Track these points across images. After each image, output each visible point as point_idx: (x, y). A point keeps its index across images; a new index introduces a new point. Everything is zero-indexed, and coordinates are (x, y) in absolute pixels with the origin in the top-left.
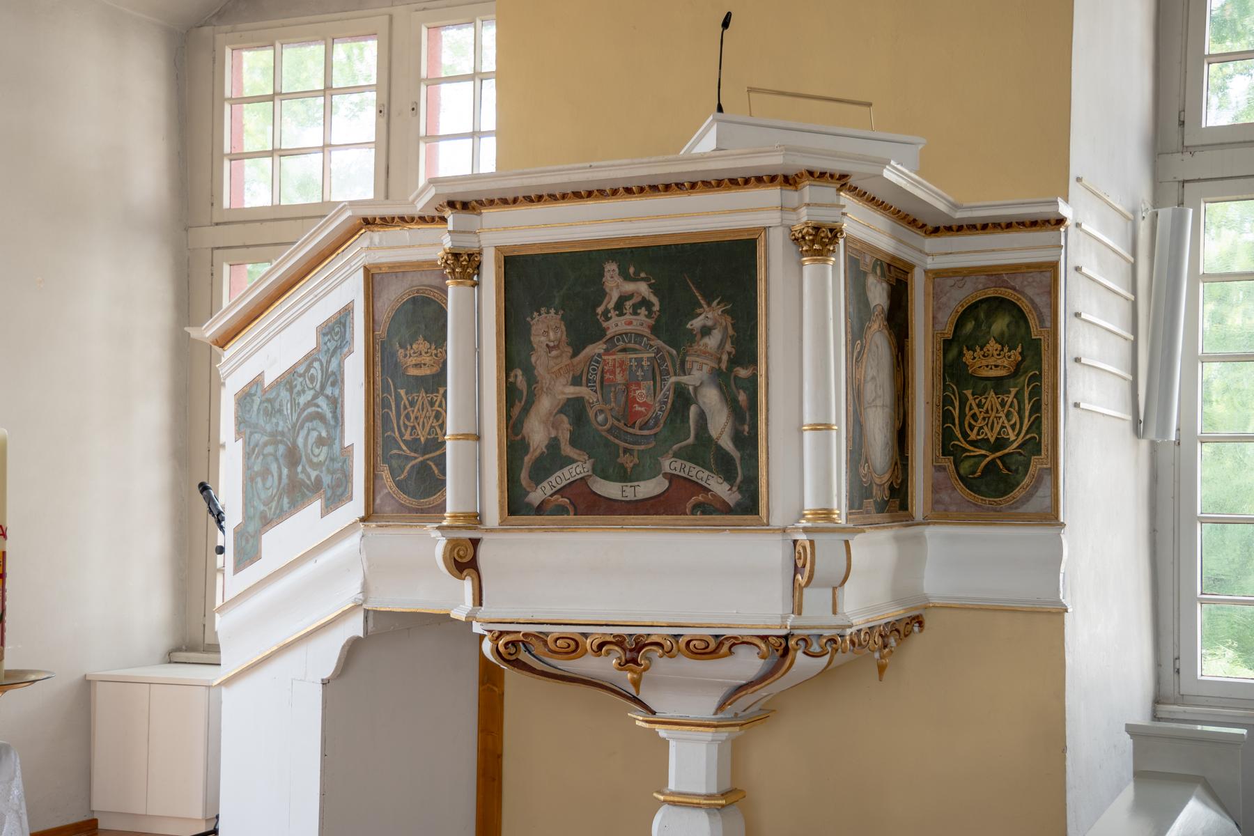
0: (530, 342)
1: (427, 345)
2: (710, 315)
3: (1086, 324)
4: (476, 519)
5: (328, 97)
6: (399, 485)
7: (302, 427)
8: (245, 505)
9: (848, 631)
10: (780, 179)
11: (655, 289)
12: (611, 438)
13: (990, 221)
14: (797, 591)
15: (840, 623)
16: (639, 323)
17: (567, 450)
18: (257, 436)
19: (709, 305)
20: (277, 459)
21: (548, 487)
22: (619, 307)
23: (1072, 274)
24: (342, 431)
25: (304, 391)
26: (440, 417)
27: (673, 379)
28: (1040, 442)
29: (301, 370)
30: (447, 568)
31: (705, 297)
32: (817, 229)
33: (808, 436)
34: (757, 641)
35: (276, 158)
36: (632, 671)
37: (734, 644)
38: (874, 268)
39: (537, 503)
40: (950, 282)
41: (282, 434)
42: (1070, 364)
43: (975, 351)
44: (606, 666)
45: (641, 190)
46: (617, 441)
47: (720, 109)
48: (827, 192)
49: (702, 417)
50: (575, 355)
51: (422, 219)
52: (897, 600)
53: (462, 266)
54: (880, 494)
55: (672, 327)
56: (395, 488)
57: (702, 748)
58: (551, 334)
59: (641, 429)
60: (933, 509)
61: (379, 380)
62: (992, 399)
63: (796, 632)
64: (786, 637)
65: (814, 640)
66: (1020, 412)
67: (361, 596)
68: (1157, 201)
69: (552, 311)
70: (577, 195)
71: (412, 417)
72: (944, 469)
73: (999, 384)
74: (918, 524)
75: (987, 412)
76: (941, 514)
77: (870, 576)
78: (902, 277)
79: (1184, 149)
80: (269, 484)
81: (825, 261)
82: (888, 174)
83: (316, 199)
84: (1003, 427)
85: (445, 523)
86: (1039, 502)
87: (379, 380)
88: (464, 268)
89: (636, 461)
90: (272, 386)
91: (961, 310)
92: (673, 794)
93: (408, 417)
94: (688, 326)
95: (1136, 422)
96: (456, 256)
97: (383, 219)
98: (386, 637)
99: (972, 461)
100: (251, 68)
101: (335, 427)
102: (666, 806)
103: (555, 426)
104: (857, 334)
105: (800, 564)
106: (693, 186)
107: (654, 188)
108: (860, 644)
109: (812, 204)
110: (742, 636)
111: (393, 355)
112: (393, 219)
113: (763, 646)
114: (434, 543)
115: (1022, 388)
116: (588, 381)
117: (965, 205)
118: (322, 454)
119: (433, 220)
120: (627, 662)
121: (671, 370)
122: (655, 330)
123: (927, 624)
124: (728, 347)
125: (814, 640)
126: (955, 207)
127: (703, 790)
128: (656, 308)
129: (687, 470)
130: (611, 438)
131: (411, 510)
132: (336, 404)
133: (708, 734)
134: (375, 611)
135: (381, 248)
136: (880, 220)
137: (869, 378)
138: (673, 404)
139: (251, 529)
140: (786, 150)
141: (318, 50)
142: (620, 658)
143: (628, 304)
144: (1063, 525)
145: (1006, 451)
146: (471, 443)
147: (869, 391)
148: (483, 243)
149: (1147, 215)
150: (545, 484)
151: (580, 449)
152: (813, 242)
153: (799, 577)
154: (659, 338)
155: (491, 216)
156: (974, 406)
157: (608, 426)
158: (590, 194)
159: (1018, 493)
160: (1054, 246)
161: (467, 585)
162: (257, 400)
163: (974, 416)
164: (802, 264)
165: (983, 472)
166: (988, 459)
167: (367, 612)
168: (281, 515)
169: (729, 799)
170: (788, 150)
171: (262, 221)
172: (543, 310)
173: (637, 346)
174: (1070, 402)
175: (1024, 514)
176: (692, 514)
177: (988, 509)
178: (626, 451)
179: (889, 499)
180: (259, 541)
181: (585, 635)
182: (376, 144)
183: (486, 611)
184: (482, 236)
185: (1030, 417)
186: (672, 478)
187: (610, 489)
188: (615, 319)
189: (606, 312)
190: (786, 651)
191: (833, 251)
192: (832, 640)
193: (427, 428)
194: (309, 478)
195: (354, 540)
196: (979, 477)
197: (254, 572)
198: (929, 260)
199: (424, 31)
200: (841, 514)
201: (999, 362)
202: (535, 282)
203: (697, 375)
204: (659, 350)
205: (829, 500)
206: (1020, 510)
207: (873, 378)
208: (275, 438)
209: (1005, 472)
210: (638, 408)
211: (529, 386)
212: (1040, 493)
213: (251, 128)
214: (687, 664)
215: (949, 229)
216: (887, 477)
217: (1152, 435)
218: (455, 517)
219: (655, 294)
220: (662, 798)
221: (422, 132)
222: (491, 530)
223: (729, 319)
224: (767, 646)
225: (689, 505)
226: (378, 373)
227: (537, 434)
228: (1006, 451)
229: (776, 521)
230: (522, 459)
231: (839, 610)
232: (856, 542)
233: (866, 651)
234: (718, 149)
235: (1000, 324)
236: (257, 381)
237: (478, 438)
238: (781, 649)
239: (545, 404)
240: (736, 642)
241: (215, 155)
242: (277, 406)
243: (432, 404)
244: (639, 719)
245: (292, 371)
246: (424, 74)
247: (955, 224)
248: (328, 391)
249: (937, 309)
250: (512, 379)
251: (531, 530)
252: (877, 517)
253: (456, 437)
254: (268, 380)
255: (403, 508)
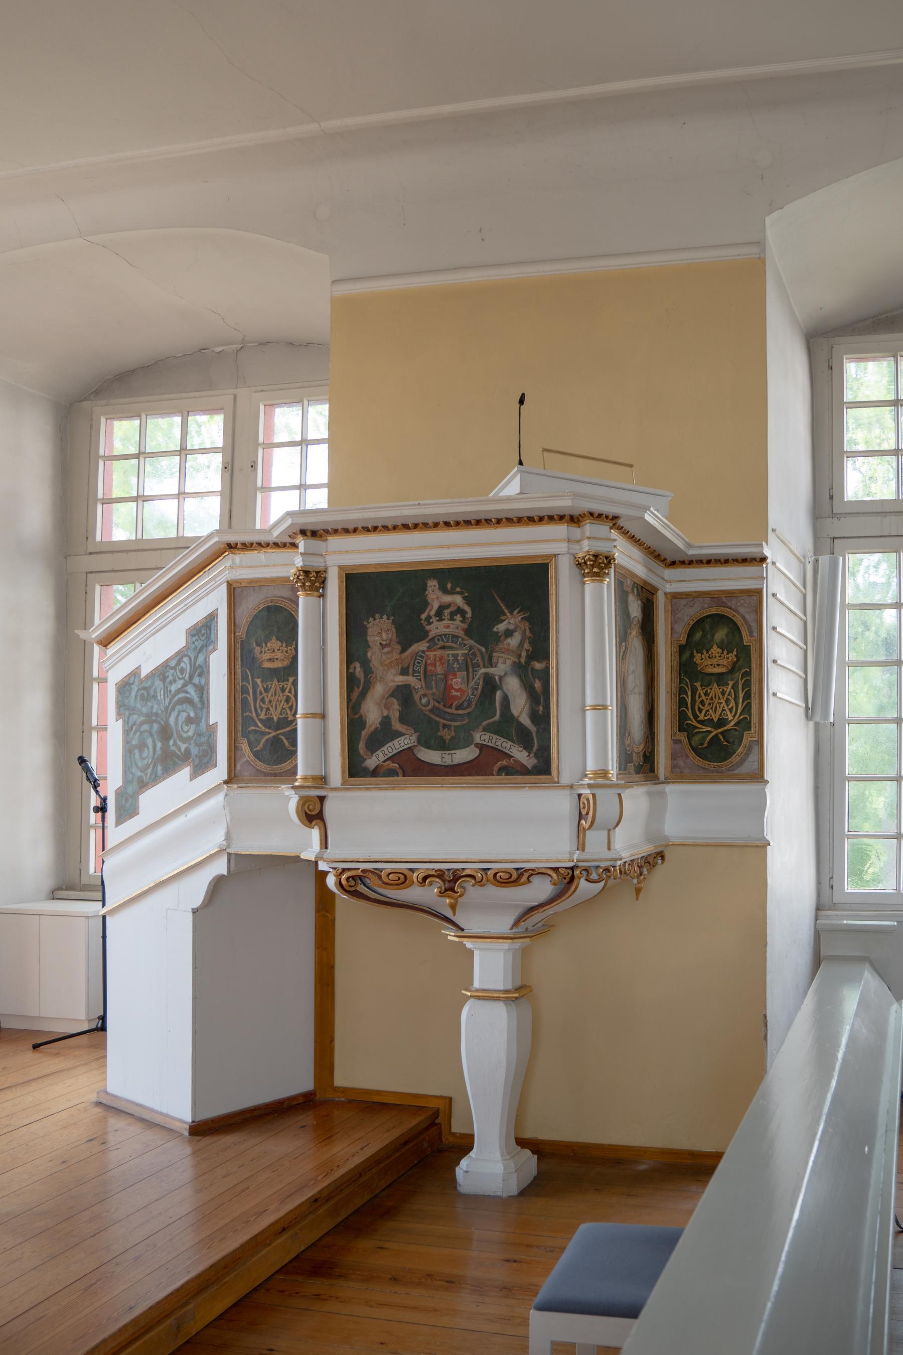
0: (367, 641)
1: (279, 643)
2: (512, 621)
3: (779, 636)
4: (322, 780)
5: (183, 457)
6: (256, 755)
7: (173, 709)
8: (125, 772)
9: (619, 863)
10: (567, 518)
11: (468, 601)
12: (433, 716)
13: (713, 558)
14: (580, 832)
15: (614, 856)
16: (456, 626)
17: (397, 726)
18: (135, 717)
19: (511, 613)
20: (151, 735)
21: (381, 755)
22: (439, 614)
23: (770, 598)
24: (208, 712)
25: (175, 681)
26: (291, 701)
27: (483, 670)
28: (750, 721)
29: (173, 663)
30: (300, 819)
31: (507, 607)
32: (596, 556)
33: (589, 714)
34: (550, 872)
35: (140, 503)
36: (449, 897)
37: (532, 875)
38: (633, 589)
39: (372, 767)
40: (683, 602)
41: (157, 714)
42: (771, 665)
43: (702, 654)
44: (428, 895)
45: (457, 524)
46: (437, 719)
47: (521, 463)
48: (603, 529)
49: (506, 700)
50: (403, 651)
51: (276, 545)
52: (649, 839)
53: (310, 581)
54: (637, 760)
55: (482, 630)
56: (252, 757)
57: (501, 955)
58: (384, 635)
59: (457, 709)
60: (672, 772)
61: (239, 671)
62: (715, 689)
63: (580, 864)
64: (572, 869)
65: (593, 870)
66: (736, 699)
67: (225, 843)
68: (817, 551)
69: (385, 617)
70: (406, 527)
71: (267, 700)
72: (680, 741)
73: (720, 679)
74: (663, 783)
75: (712, 699)
76: (678, 775)
77: (634, 821)
78: (650, 597)
79: (833, 515)
80: (145, 754)
81: (602, 581)
82: (648, 517)
83: (173, 534)
84: (723, 710)
85: (297, 784)
86: (749, 766)
87: (239, 671)
88: (313, 582)
89: (453, 734)
90: (148, 677)
91: (692, 623)
92: (477, 990)
93: (263, 700)
94: (495, 629)
95: (807, 709)
96: (307, 573)
97: (244, 544)
98: (245, 875)
99: (701, 736)
100: (121, 434)
101: (202, 709)
102: (472, 1000)
103: (387, 707)
104: (623, 638)
105: (584, 812)
106: (499, 521)
107: (468, 523)
108: (625, 873)
109: (592, 539)
110: (538, 869)
111: (251, 651)
112: (252, 544)
113: (554, 875)
114: (289, 800)
115: (737, 682)
116: (414, 671)
117: (696, 544)
118: (191, 730)
119: (284, 545)
120: (446, 890)
121: (481, 665)
122: (468, 632)
123: (667, 858)
124: (526, 646)
125: (593, 870)
126: (690, 546)
127: (501, 987)
128: (469, 615)
129: (494, 741)
130: (433, 716)
131: (266, 774)
132: (203, 691)
133: (505, 945)
134: (236, 855)
135: (241, 567)
136: (636, 553)
137: (630, 672)
138: (482, 691)
139: (130, 790)
140: (575, 495)
141: (178, 420)
142: (440, 887)
143: (446, 612)
144: (767, 782)
145: (726, 728)
146: (318, 721)
147: (631, 680)
148: (329, 563)
149: (811, 559)
150: (379, 752)
151: (408, 725)
152: (593, 566)
153: (583, 822)
154: (471, 638)
155: (334, 542)
156: (702, 694)
157: (430, 707)
158: (416, 526)
159: (734, 759)
160: (759, 578)
161: (315, 834)
162: (135, 688)
163: (702, 702)
164: (584, 583)
165: (709, 743)
166: (713, 734)
167: (229, 854)
168: (156, 779)
169: (519, 994)
170: (575, 495)
171: (127, 551)
172: (377, 616)
173: (454, 645)
174: (771, 692)
175: (738, 775)
176: (498, 775)
177: (713, 772)
178: (444, 726)
179: (642, 764)
180: (136, 800)
181: (412, 870)
182: (222, 493)
183: (331, 853)
184: (328, 558)
185: (743, 702)
186: (481, 747)
187: (432, 757)
188: (436, 624)
189: (429, 618)
190: (572, 879)
191: (608, 574)
192: (607, 870)
193: (279, 710)
194: (179, 749)
195: (219, 798)
196: (706, 747)
197: (132, 826)
198: (668, 585)
199: (262, 407)
200: (613, 772)
201: (720, 662)
202: (371, 595)
203: (502, 667)
204: (471, 648)
205: (606, 764)
206: (736, 772)
207: (633, 672)
208: (150, 718)
209: (725, 743)
210: (454, 693)
211: (366, 676)
212: (750, 758)
213: (119, 479)
214: (493, 892)
215: (683, 563)
216: (642, 747)
217: (818, 718)
218: (305, 779)
219: (468, 604)
220: (469, 994)
221: (259, 484)
222: (335, 789)
223: (527, 624)
224: (558, 875)
225: (495, 768)
226: (238, 666)
227: (372, 713)
228: (726, 728)
229: (565, 779)
230: (360, 734)
231: (612, 847)
232: (626, 794)
233: (629, 877)
234: (520, 493)
235: (721, 634)
236: (135, 673)
237: (323, 716)
238: (567, 878)
239: (379, 690)
240: (533, 873)
241: (90, 500)
242: (152, 693)
243: (283, 690)
244: (451, 936)
245: (165, 665)
246: (261, 440)
247: (687, 559)
248: (196, 680)
249: (674, 623)
250: (351, 670)
251: (368, 789)
252: (636, 777)
253: (305, 716)
254: (144, 673)
255: (260, 772)
